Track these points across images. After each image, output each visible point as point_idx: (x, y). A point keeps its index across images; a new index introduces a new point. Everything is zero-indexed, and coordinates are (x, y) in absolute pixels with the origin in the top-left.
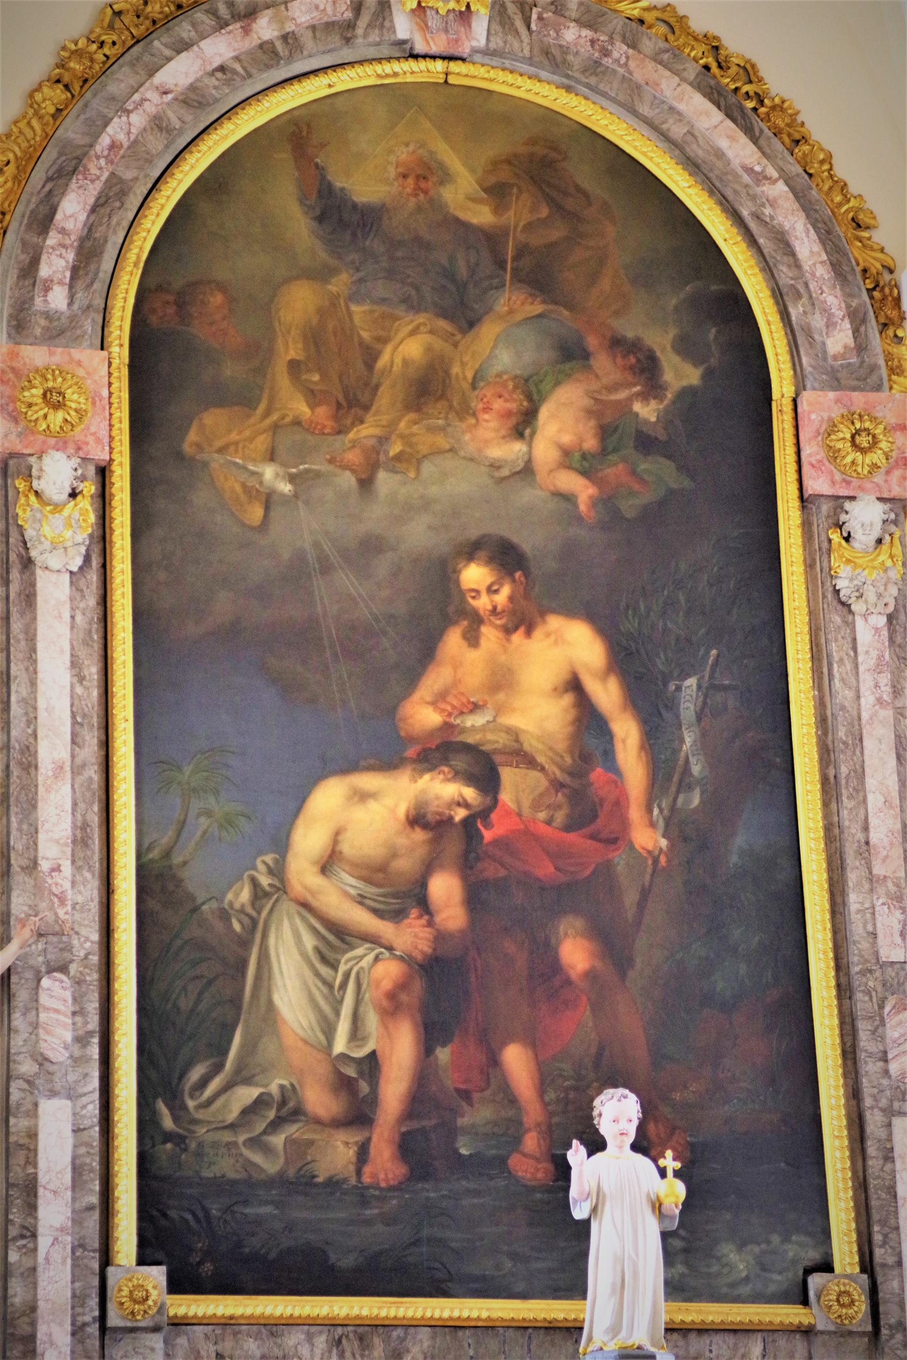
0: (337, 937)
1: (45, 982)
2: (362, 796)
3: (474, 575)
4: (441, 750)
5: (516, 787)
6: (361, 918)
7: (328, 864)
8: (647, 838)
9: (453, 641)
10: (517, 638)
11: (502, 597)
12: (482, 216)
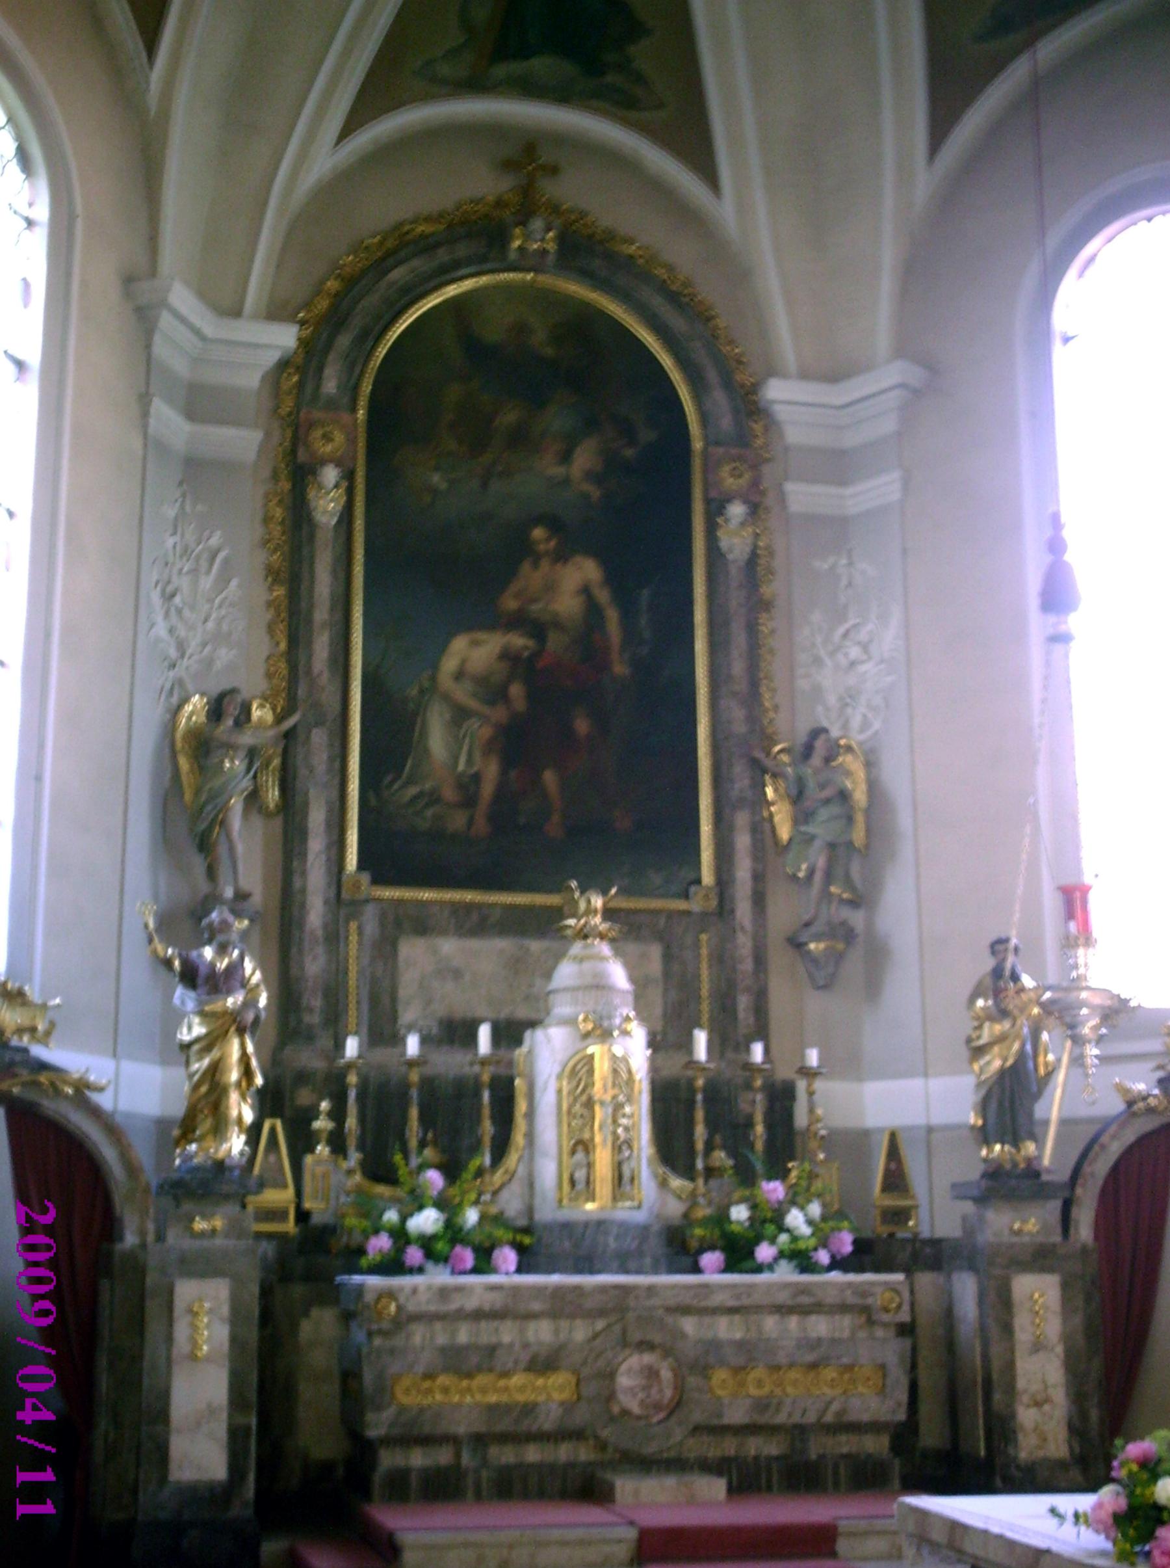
0: (460, 715)
1: (314, 731)
2: (475, 643)
3: (538, 533)
4: (517, 621)
5: (555, 642)
6: (472, 704)
7: (459, 675)
8: (620, 668)
9: (526, 567)
10: (559, 566)
11: (553, 543)
12: (549, 351)
